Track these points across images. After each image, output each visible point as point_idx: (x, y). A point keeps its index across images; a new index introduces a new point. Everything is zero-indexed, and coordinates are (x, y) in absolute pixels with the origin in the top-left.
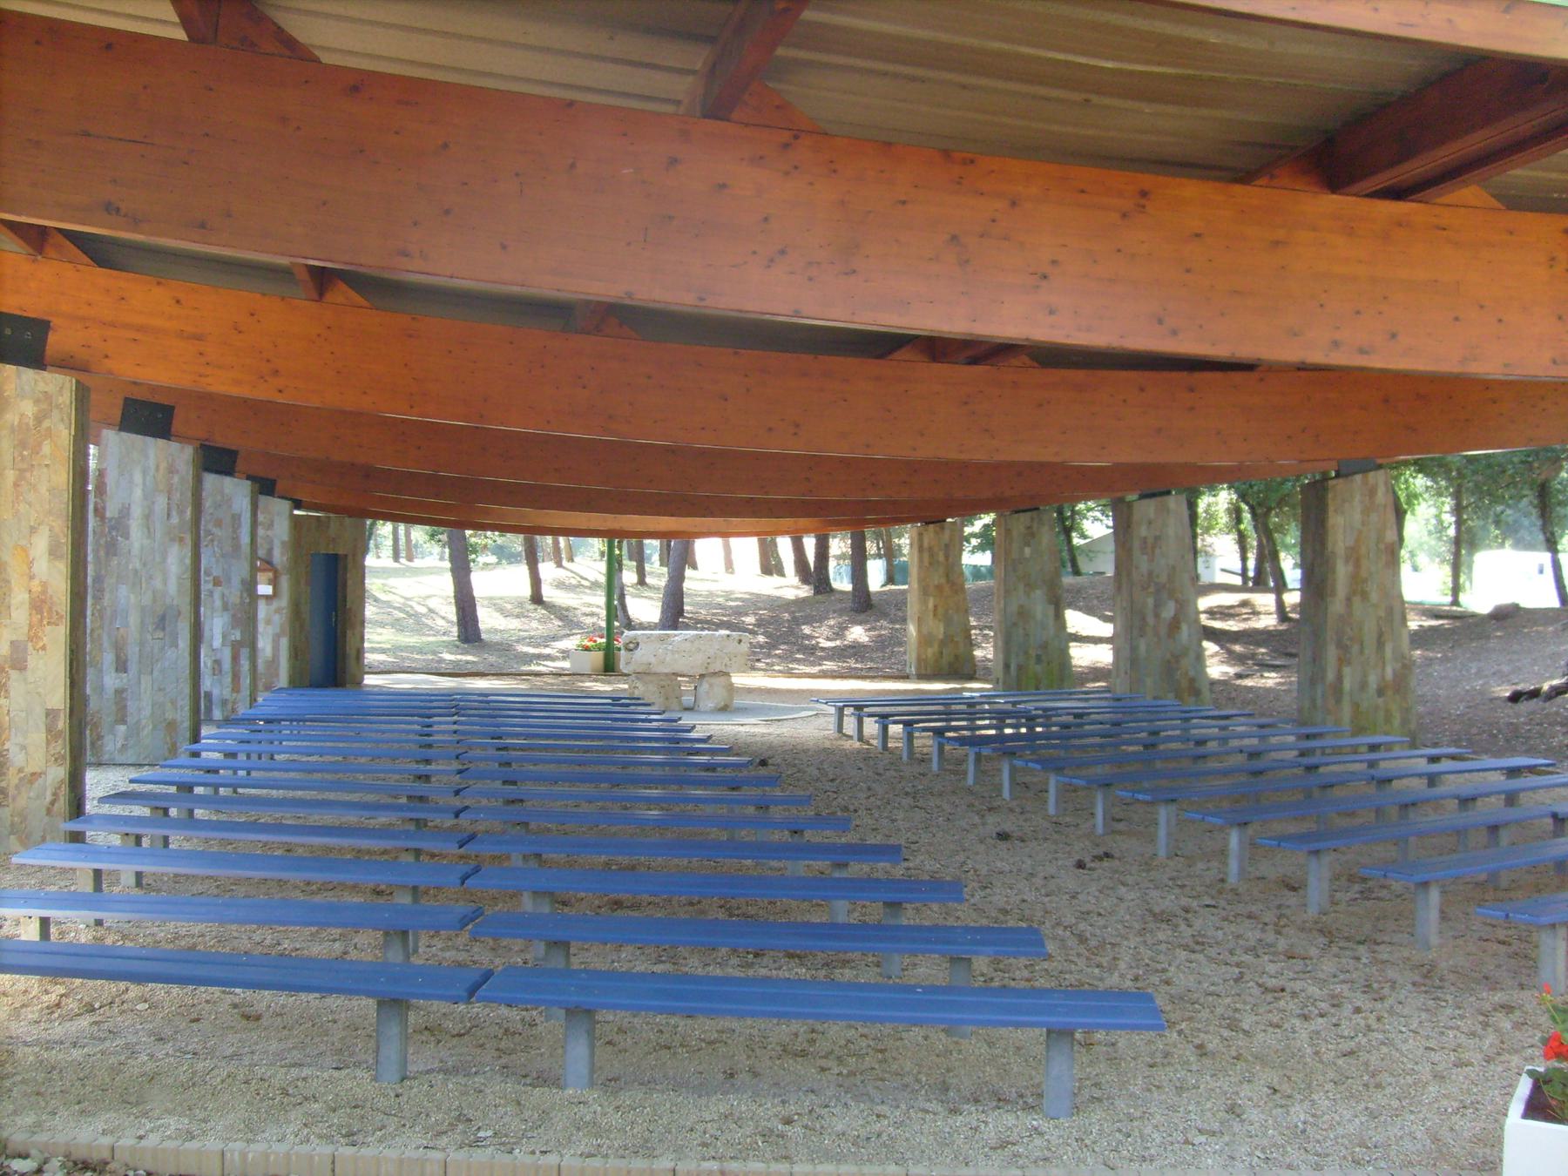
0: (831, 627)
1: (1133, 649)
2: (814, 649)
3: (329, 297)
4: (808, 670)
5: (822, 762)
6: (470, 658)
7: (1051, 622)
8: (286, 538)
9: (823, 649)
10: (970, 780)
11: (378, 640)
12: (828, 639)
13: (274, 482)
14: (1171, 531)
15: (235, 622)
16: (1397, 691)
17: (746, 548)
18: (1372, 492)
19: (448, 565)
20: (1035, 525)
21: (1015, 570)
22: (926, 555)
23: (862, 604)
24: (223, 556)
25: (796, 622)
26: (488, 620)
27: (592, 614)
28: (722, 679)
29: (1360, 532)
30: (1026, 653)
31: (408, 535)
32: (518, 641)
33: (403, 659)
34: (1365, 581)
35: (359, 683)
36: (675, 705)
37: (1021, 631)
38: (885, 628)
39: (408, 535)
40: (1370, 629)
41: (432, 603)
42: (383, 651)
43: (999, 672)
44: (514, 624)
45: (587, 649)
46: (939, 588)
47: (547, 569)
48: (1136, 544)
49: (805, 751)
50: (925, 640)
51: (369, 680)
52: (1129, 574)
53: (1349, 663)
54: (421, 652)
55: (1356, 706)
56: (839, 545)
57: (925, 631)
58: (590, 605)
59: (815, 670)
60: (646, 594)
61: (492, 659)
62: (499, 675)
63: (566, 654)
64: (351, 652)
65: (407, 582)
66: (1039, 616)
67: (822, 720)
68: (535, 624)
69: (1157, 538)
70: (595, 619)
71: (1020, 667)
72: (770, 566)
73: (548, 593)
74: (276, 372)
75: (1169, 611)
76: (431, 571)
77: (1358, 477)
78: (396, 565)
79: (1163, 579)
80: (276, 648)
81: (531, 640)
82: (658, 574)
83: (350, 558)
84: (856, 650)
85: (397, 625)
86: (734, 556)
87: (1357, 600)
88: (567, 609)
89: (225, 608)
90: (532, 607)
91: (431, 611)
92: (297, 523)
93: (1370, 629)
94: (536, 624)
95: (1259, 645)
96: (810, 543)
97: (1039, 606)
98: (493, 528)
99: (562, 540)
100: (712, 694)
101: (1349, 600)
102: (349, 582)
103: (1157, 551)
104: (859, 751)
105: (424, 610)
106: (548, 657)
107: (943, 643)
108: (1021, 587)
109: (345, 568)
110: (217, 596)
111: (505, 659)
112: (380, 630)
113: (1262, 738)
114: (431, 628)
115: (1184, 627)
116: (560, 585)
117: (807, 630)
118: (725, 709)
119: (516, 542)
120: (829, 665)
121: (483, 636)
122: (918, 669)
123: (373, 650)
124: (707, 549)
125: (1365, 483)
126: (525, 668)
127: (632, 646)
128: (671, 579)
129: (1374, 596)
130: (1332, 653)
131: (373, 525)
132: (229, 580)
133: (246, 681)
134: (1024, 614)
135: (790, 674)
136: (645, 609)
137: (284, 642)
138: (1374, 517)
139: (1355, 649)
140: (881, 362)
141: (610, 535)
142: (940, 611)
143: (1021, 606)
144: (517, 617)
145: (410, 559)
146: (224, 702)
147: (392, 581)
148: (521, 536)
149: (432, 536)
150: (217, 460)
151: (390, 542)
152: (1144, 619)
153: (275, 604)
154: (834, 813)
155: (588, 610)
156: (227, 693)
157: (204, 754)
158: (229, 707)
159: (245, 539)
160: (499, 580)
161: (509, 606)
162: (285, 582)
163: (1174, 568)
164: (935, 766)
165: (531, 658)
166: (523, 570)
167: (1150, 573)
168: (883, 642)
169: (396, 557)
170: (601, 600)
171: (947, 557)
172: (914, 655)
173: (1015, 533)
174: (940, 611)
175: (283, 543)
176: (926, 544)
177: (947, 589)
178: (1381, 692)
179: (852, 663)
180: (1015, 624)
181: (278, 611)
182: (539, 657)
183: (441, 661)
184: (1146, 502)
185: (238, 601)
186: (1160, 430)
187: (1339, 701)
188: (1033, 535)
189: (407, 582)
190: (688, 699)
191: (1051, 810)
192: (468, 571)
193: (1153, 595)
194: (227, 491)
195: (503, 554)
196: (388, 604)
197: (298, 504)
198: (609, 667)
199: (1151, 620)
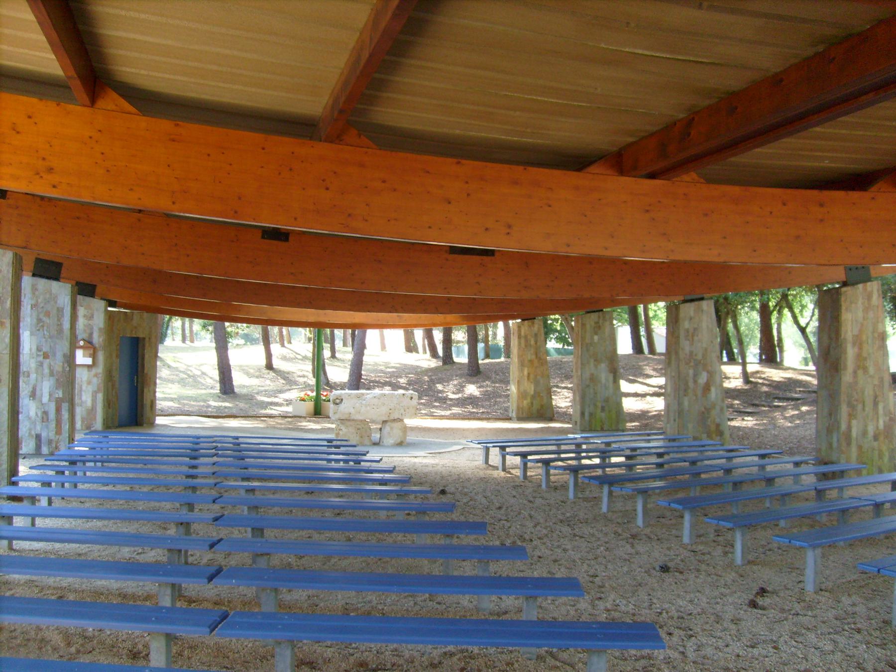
0: (455, 386)
1: (680, 404)
2: (444, 400)
3: (101, 103)
4: (443, 413)
5: (484, 491)
6: (227, 404)
7: (611, 385)
8: (102, 325)
9: (451, 400)
10: (604, 509)
11: (166, 391)
12: (453, 393)
13: (94, 287)
14: (704, 325)
15: (58, 385)
16: (886, 437)
17: (395, 336)
18: (869, 297)
19: (214, 345)
20: (601, 322)
21: (588, 350)
22: (523, 341)
23: (474, 371)
24: (51, 337)
25: (432, 382)
26: (239, 380)
27: (304, 376)
28: (397, 425)
29: (862, 325)
30: (595, 405)
31: (191, 327)
32: (258, 393)
33: (184, 405)
34: (865, 359)
35: (152, 424)
36: (367, 442)
37: (592, 391)
38: (489, 386)
39: (191, 327)
40: (869, 392)
41: (204, 369)
42: (172, 400)
43: (577, 417)
44: (254, 382)
45: (303, 400)
46: (531, 361)
47: (275, 348)
48: (682, 334)
49: (469, 480)
50: (522, 395)
51: (159, 420)
52: (677, 353)
53: (856, 418)
54: (196, 400)
55: (860, 447)
56: (460, 335)
57: (522, 389)
58: (302, 371)
59: (448, 413)
60: (336, 364)
61: (242, 405)
62: (246, 417)
63: (289, 402)
64: (147, 402)
65: (185, 355)
66: (603, 381)
67: (467, 453)
68: (268, 382)
69: (695, 329)
70: (305, 379)
71: (591, 414)
72: (411, 347)
73: (276, 363)
74: (50, 170)
75: (703, 378)
76: (204, 349)
77: (860, 286)
78: (184, 345)
79: (699, 357)
80: (94, 400)
81: (267, 393)
82: (346, 354)
83: (147, 339)
84: (472, 400)
85: (182, 382)
86: (386, 342)
87: (860, 373)
88: (288, 373)
89: (52, 374)
90: (267, 371)
91: (203, 373)
92: (110, 316)
93: (869, 392)
94: (269, 382)
95: (734, 398)
96: (438, 335)
97: (604, 375)
98: (242, 321)
99: (285, 330)
100: (392, 434)
101: (855, 372)
102: (146, 356)
103: (696, 338)
104: (507, 480)
105: (199, 373)
106: (276, 404)
107: (533, 397)
108: (592, 361)
109: (144, 346)
110: (46, 366)
111: (250, 407)
112: (170, 385)
113: (729, 459)
114: (203, 385)
115: (713, 389)
116: (284, 358)
117: (439, 387)
118: (400, 444)
119: (256, 331)
120: (456, 410)
121: (236, 390)
122: (517, 413)
123: (165, 399)
124: (372, 336)
125: (865, 289)
126: (263, 412)
127: (338, 401)
128: (355, 355)
129: (871, 370)
130: (844, 410)
131: (170, 320)
132: (54, 354)
133: (66, 427)
134: (593, 379)
135: (432, 416)
136: (338, 373)
137: (100, 396)
138: (871, 315)
139: (860, 407)
140: (581, 174)
141: (318, 326)
142: (532, 376)
143: (592, 375)
144: (257, 377)
145: (192, 341)
146: (50, 442)
147: (180, 355)
148: (260, 327)
149: (204, 326)
150: (85, 289)
151: (180, 332)
152: (686, 384)
153: (94, 371)
154: (514, 542)
155: (301, 374)
156: (52, 435)
157: (21, 484)
158: (54, 445)
159: (67, 325)
160: (245, 354)
161: (252, 371)
162: (101, 356)
163: (706, 349)
164: (571, 495)
165: (265, 405)
166: (261, 348)
167: (691, 353)
168: (489, 395)
169: (184, 340)
170: (308, 367)
171: (536, 343)
172: (515, 405)
173: (588, 327)
174: (532, 376)
175: (100, 329)
176: (523, 334)
177: (536, 361)
178: (876, 438)
179: (470, 408)
180: (588, 386)
181: (96, 375)
182: (272, 404)
183: (209, 406)
184: (688, 305)
185: (60, 369)
186: (798, 237)
187: (849, 444)
188: (599, 327)
189: (185, 355)
190: (376, 436)
191: (686, 539)
192: (226, 349)
193: (686, 370)
194: (54, 291)
195: (248, 338)
196: (176, 369)
197: (112, 304)
198: (318, 412)
199: (691, 384)
